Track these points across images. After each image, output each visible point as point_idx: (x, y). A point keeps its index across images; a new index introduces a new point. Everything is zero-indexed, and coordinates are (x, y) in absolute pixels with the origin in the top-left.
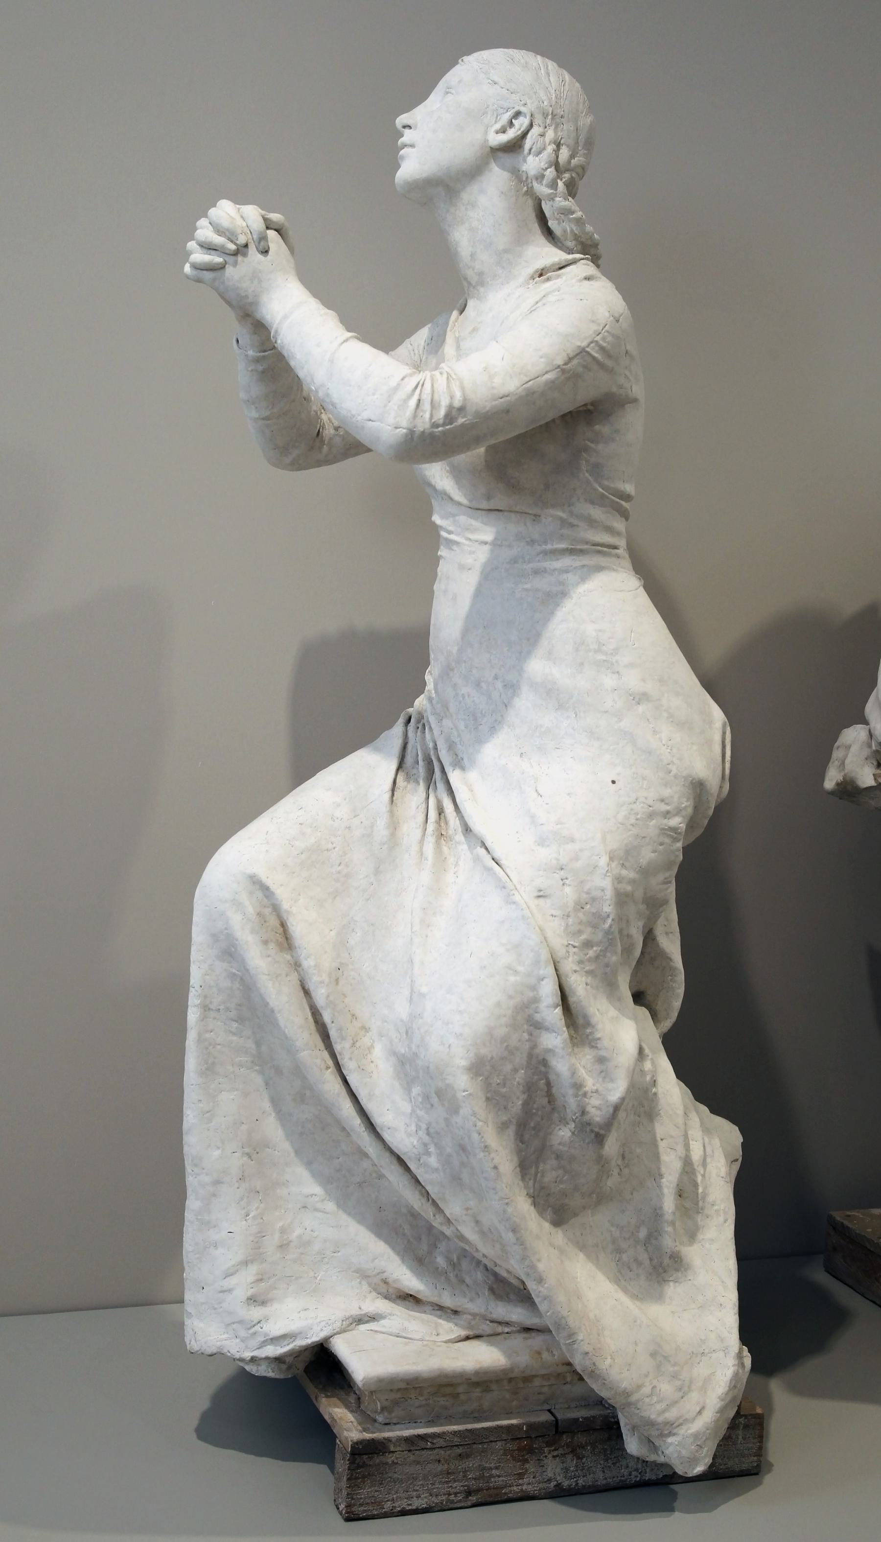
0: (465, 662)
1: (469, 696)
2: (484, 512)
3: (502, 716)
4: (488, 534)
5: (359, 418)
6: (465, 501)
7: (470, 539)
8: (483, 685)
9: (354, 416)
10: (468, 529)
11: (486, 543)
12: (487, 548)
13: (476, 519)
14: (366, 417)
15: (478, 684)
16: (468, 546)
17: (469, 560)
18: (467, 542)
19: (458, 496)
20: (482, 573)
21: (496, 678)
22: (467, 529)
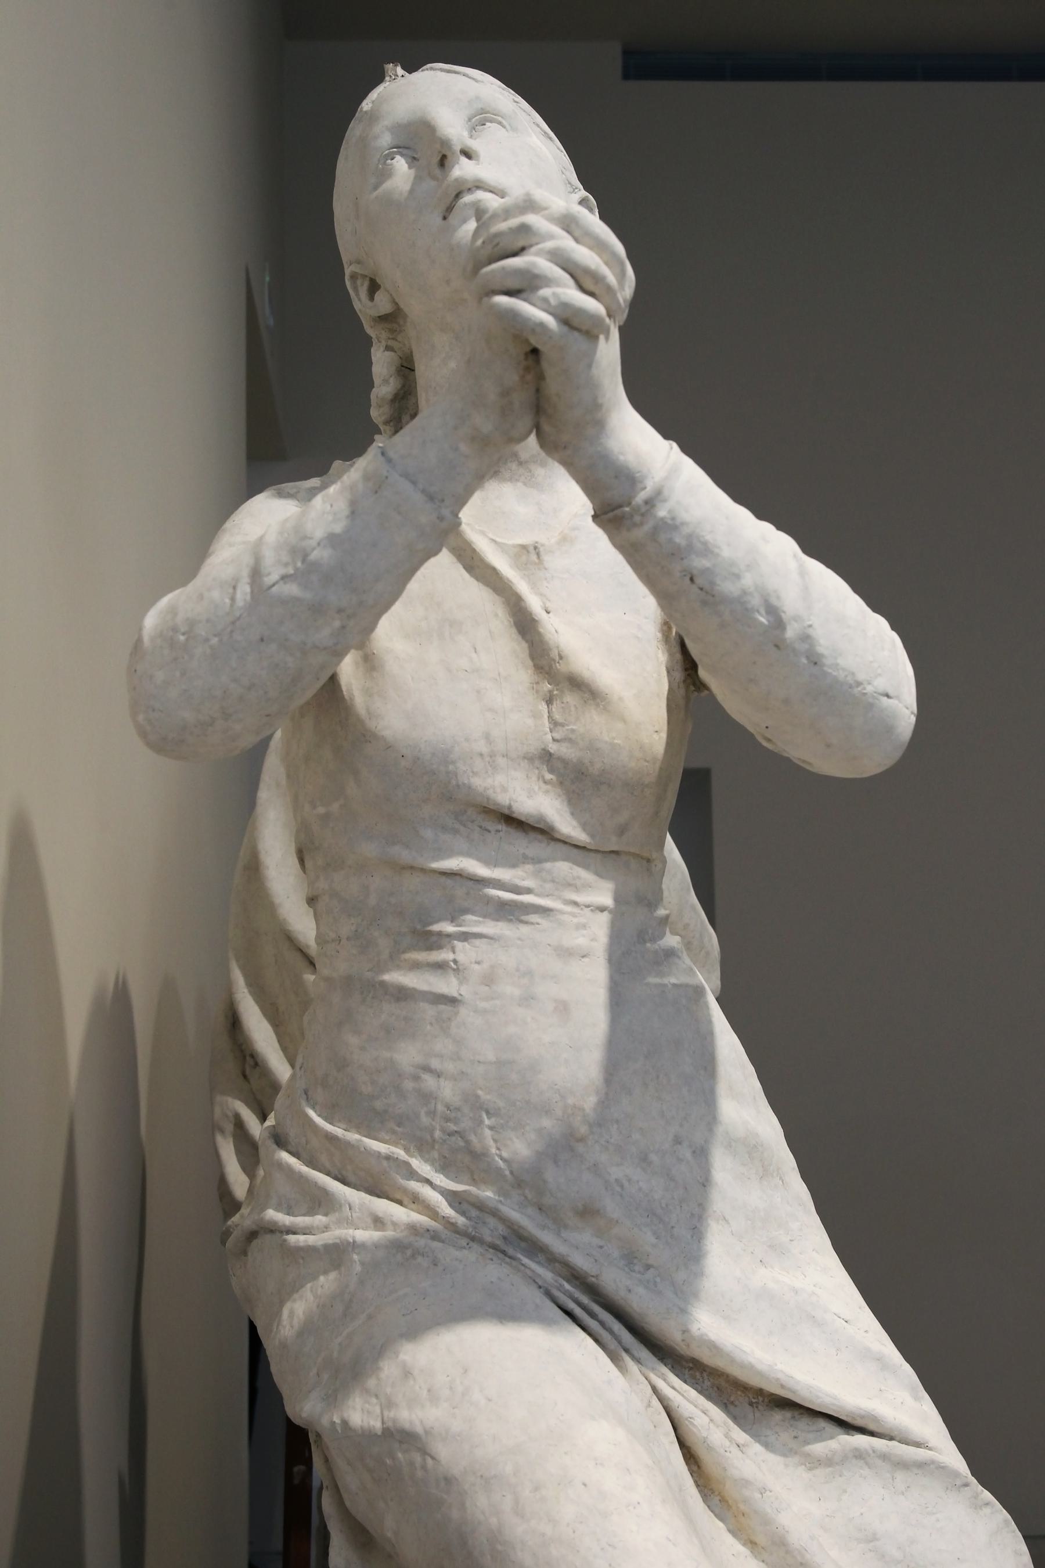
0: (617, 1121)
1: (629, 1180)
2: (599, 856)
3: (700, 1205)
4: (603, 895)
5: (869, 689)
6: (580, 836)
7: (576, 904)
8: (653, 1157)
9: (859, 684)
10: (570, 885)
11: (602, 909)
12: (605, 918)
13: (586, 867)
14: (881, 689)
15: (644, 1159)
16: (574, 915)
17: (580, 940)
18: (569, 909)
19: (567, 825)
20: (610, 961)
21: (678, 1141)
22: (571, 885)
